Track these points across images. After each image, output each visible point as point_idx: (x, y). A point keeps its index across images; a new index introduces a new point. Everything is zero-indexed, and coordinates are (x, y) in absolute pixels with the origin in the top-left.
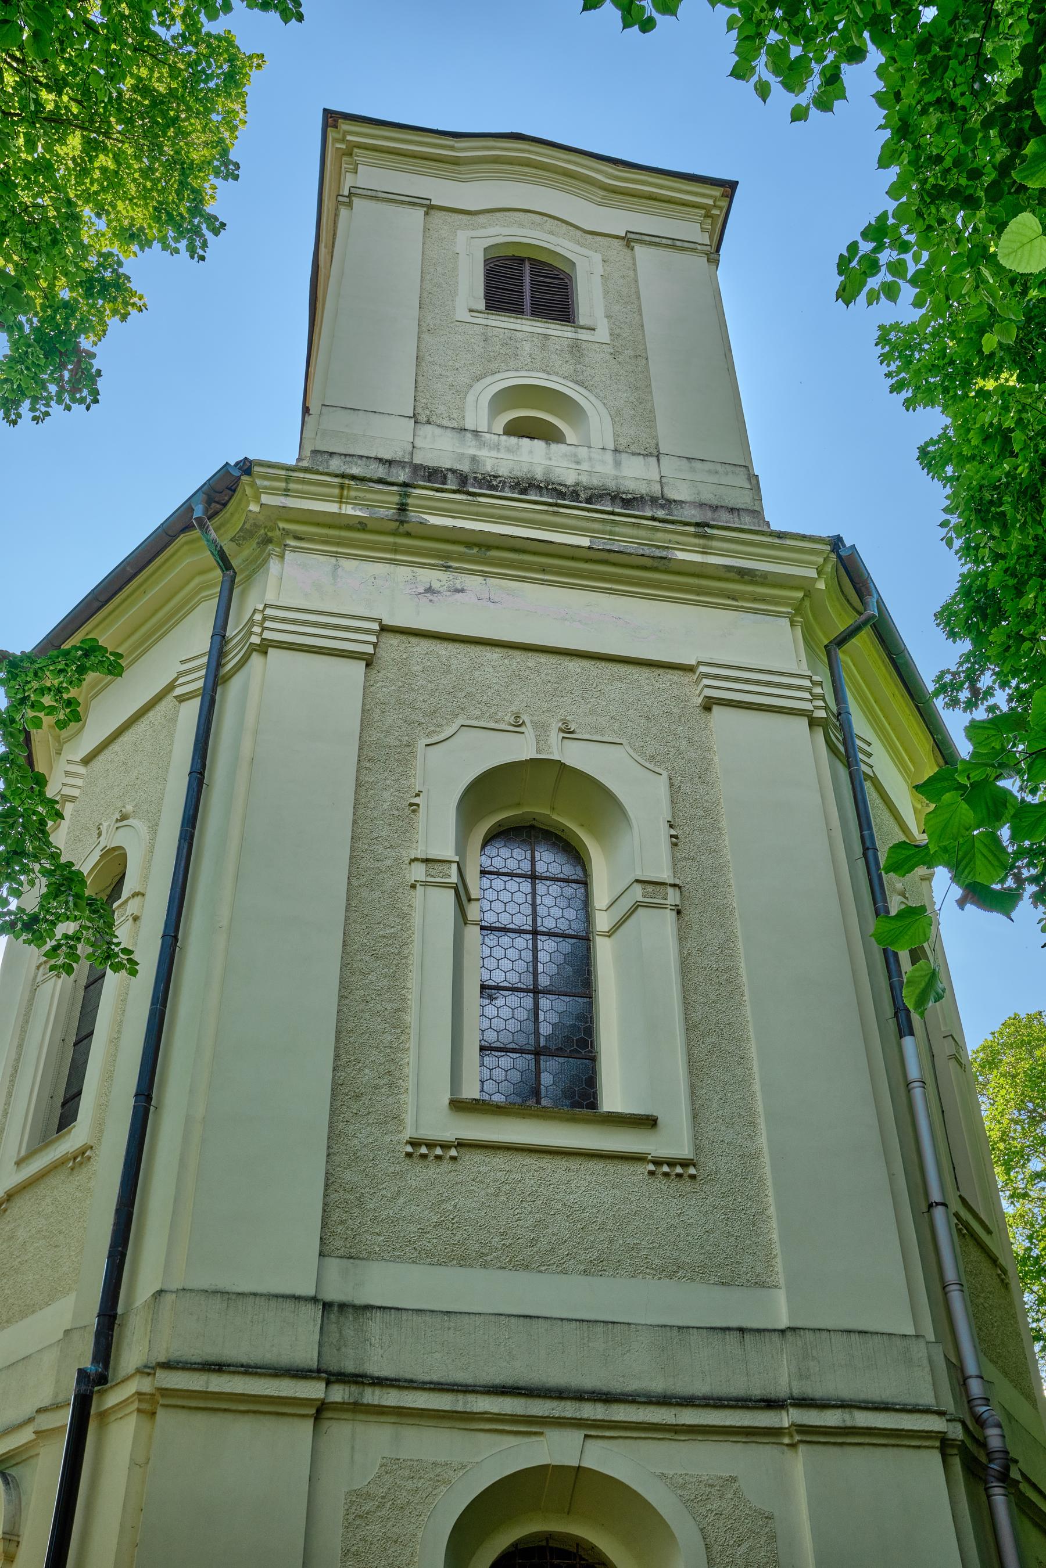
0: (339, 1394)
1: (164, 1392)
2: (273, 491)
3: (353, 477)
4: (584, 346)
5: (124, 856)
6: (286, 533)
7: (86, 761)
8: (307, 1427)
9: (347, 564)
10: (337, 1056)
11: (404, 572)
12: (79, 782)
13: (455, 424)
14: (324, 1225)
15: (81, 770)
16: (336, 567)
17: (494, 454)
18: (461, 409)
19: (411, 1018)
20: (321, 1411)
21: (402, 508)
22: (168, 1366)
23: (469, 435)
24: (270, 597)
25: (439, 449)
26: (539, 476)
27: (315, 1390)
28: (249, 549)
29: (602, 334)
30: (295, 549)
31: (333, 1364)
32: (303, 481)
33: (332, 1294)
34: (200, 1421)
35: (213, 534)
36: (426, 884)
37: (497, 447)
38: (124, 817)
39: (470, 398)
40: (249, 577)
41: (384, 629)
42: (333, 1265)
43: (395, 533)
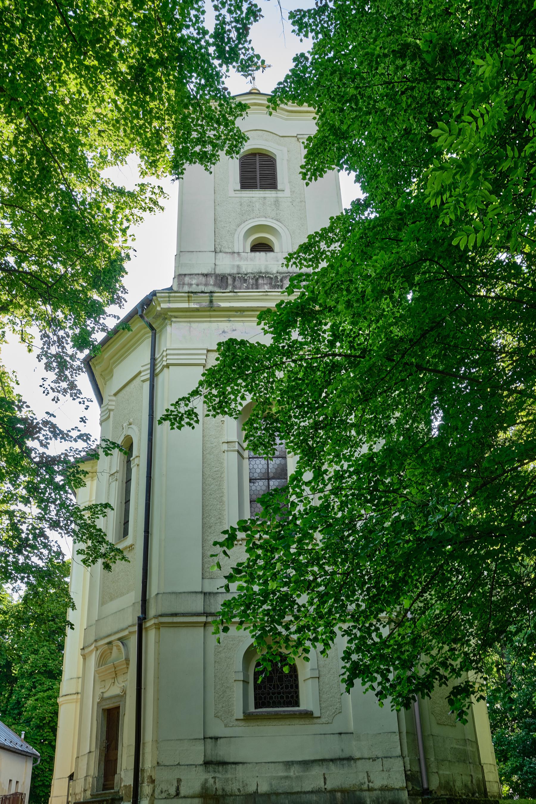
0: (210, 619)
1: (162, 623)
2: (164, 302)
3: (192, 292)
4: (280, 200)
5: (131, 438)
6: (172, 316)
7: (115, 395)
8: (202, 629)
9: (194, 325)
10: (203, 515)
11: (214, 325)
12: (114, 403)
13: (230, 251)
14: (203, 569)
15: (114, 398)
16: (190, 327)
17: (246, 263)
18: (233, 242)
19: (225, 499)
20: (205, 624)
21: (211, 301)
22: (161, 616)
23: (236, 255)
24: (168, 346)
25: (226, 265)
26: (263, 271)
27: (203, 619)
28: (159, 321)
29: (287, 193)
30: (175, 322)
31: (208, 610)
32: (175, 297)
33: (207, 590)
34: (172, 630)
35: (146, 319)
36: (228, 451)
37: (247, 259)
38: (130, 424)
39: (236, 236)
40: (161, 331)
41: (208, 351)
42: (206, 581)
43: (209, 311)
